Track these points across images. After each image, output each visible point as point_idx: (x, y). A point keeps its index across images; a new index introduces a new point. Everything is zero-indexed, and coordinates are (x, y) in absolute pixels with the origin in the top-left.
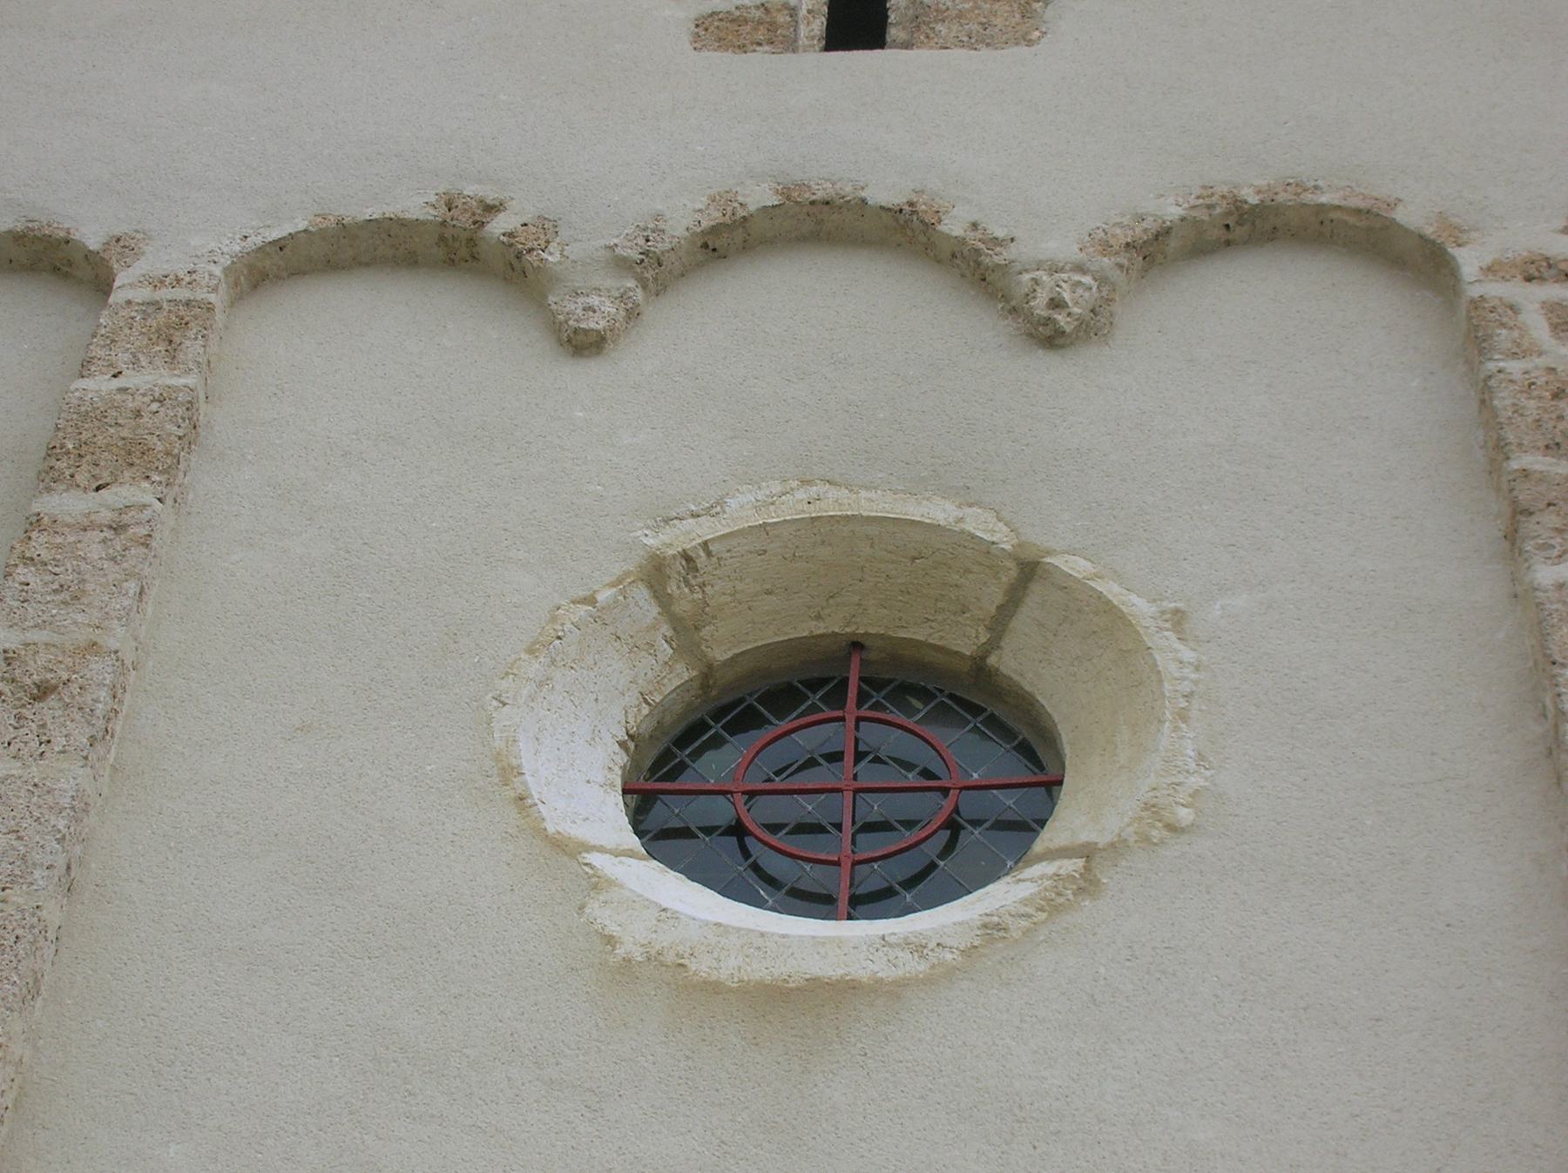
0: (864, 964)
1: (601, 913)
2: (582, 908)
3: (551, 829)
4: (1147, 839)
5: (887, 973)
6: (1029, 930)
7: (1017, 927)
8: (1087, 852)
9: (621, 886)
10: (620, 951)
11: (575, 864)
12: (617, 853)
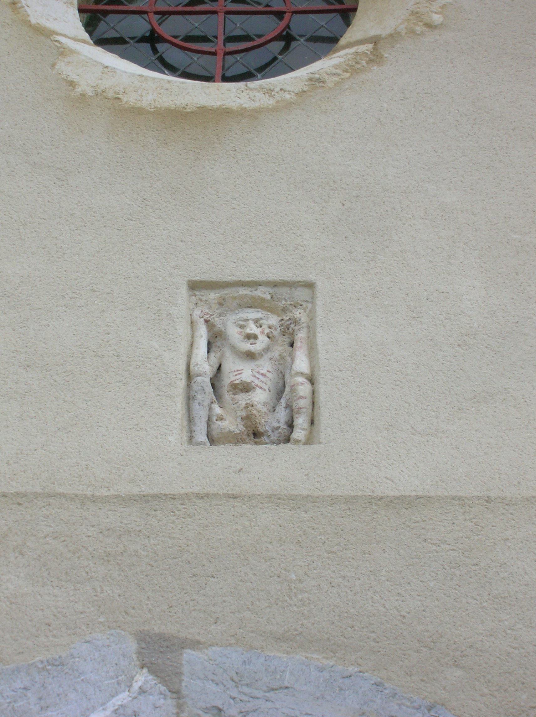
0: (234, 99)
1: (65, 68)
2: (53, 66)
3: (33, 21)
4: (413, 32)
5: (248, 104)
6: (338, 83)
7: (331, 81)
8: (375, 41)
9: (79, 53)
10: (79, 90)
11: (49, 41)
12: (75, 39)
